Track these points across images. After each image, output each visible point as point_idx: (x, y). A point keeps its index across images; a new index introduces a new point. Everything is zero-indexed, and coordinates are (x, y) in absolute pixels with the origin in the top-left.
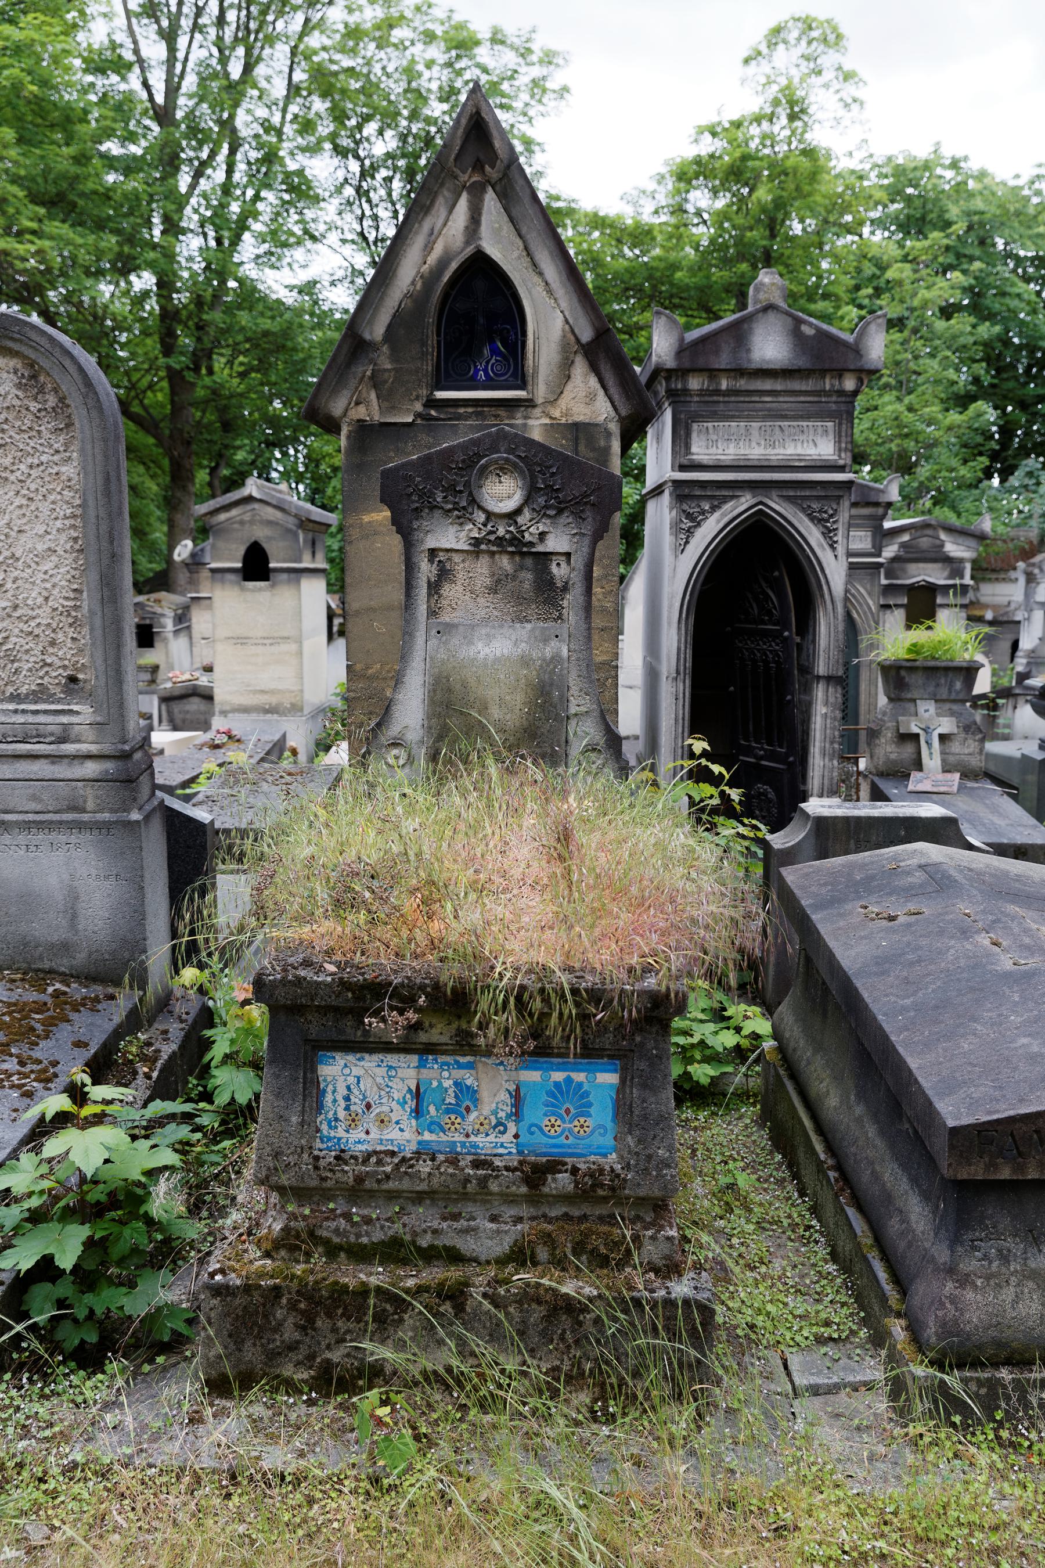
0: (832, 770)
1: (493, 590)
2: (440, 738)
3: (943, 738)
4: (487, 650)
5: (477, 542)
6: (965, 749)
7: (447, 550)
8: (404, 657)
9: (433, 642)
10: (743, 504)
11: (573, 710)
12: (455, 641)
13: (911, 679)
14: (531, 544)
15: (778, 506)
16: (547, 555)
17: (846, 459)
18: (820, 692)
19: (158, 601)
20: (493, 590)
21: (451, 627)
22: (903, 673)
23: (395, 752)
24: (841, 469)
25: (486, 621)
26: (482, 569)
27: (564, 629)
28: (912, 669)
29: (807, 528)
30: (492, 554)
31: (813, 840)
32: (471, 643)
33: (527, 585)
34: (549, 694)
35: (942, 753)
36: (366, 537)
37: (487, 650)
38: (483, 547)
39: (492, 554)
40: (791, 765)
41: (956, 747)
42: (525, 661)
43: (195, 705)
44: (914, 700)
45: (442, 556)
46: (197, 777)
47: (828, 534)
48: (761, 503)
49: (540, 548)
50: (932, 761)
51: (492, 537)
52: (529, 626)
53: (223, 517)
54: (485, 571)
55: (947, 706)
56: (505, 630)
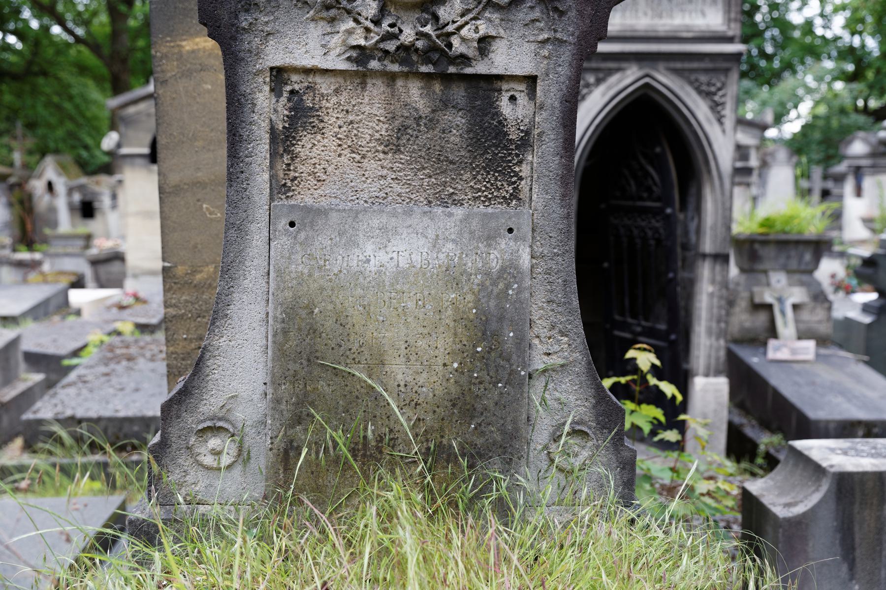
0: (718, 350)
1: (393, 146)
2: (298, 419)
3: (796, 307)
4: (383, 257)
5: (362, 55)
6: (815, 317)
7: (308, 71)
8: (229, 269)
9: (282, 243)
10: (627, 79)
11: (539, 362)
12: (323, 240)
13: (768, 252)
14: (464, 59)
15: (665, 80)
16: (492, 82)
17: (735, 30)
18: (706, 271)
19: (97, 183)
20: (393, 146)
21: (315, 213)
22: (757, 246)
23: (214, 442)
24: (730, 40)
25: (380, 201)
26: (371, 108)
27: (523, 218)
28: (765, 243)
29: (694, 101)
30: (391, 78)
31: (832, 505)
32: (352, 243)
33: (455, 137)
34: (496, 335)
35: (797, 321)
36: (187, 74)
37: (383, 257)
38: (374, 64)
39: (391, 78)
40: (673, 343)
41: (805, 315)
42: (452, 277)
43: (115, 267)
44: (765, 272)
45: (297, 82)
46: (85, 346)
47: (716, 107)
48: (647, 76)
49: (480, 68)
50: (786, 327)
51: (391, 46)
52: (459, 212)
53: (132, 110)
54: (378, 110)
55: (797, 277)
56: (414, 220)
